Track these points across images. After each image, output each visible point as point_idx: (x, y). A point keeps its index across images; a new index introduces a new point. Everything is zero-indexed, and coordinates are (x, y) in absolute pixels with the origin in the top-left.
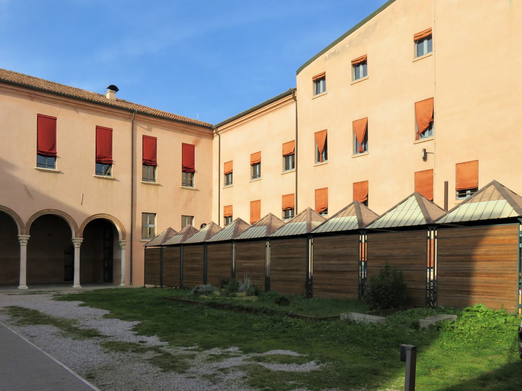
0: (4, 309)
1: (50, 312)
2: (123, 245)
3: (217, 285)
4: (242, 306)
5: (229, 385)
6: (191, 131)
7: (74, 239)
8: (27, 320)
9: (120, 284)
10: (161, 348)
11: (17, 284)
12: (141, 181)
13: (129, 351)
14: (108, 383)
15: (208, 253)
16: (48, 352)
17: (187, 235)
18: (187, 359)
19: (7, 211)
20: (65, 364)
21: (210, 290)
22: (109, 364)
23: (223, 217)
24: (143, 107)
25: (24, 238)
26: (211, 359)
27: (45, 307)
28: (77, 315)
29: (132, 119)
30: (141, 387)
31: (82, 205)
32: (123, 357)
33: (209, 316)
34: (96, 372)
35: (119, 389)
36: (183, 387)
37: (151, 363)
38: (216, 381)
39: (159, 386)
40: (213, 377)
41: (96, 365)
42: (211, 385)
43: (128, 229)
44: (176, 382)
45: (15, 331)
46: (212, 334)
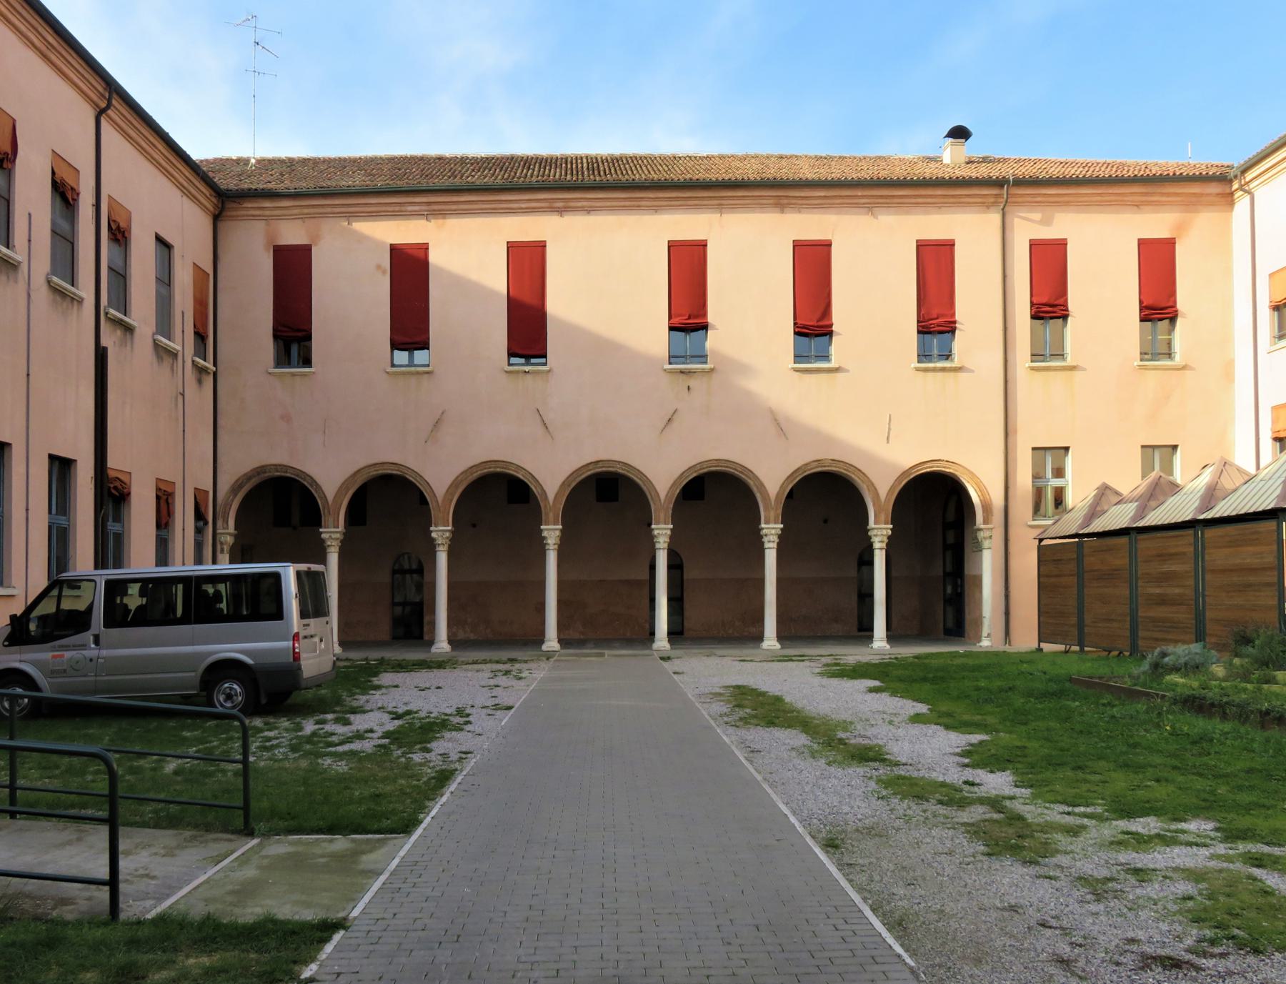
0: (722, 692)
1: (805, 702)
2: (985, 538)
3: (1221, 648)
4: (1278, 712)
5: (1134, 910)
6: (1164, 199)
7: (873, 529)
8: (755, 717)
9: (980, 641)
10: (1008, 803)
11: (759, 638)
12: (1027, 365)
13: (932, 801)
14: (860, 861)
15: (1206, 551)
16: (771, 786)
17: (1148, 501)
18: (1059, 834)
19: (740, 472)
20: (794, 813)
21: (1198, 659)
22: (878, 824)
23: (1271, 441)
24: (1032, 164)
25: (771, 530)
26: (1120, 843)
27: (799, 691)
28: (856, 713)
29: (1002, 202)
30: (924, 879)
31: (888, 442)
32: (914, 812)
33: (1174, 733)
34: (846, 836)
35: (878, 877)
36: (1019, 895)
37: (968, 832)
38: (1105, 895)
39: (964, 883)
40: (1104, 884)
41: (851, 823)
42: (1089, 903)
43: (997, 499)
44: (1006, 881)
45: (729, 737)
46: (1158, 781)
